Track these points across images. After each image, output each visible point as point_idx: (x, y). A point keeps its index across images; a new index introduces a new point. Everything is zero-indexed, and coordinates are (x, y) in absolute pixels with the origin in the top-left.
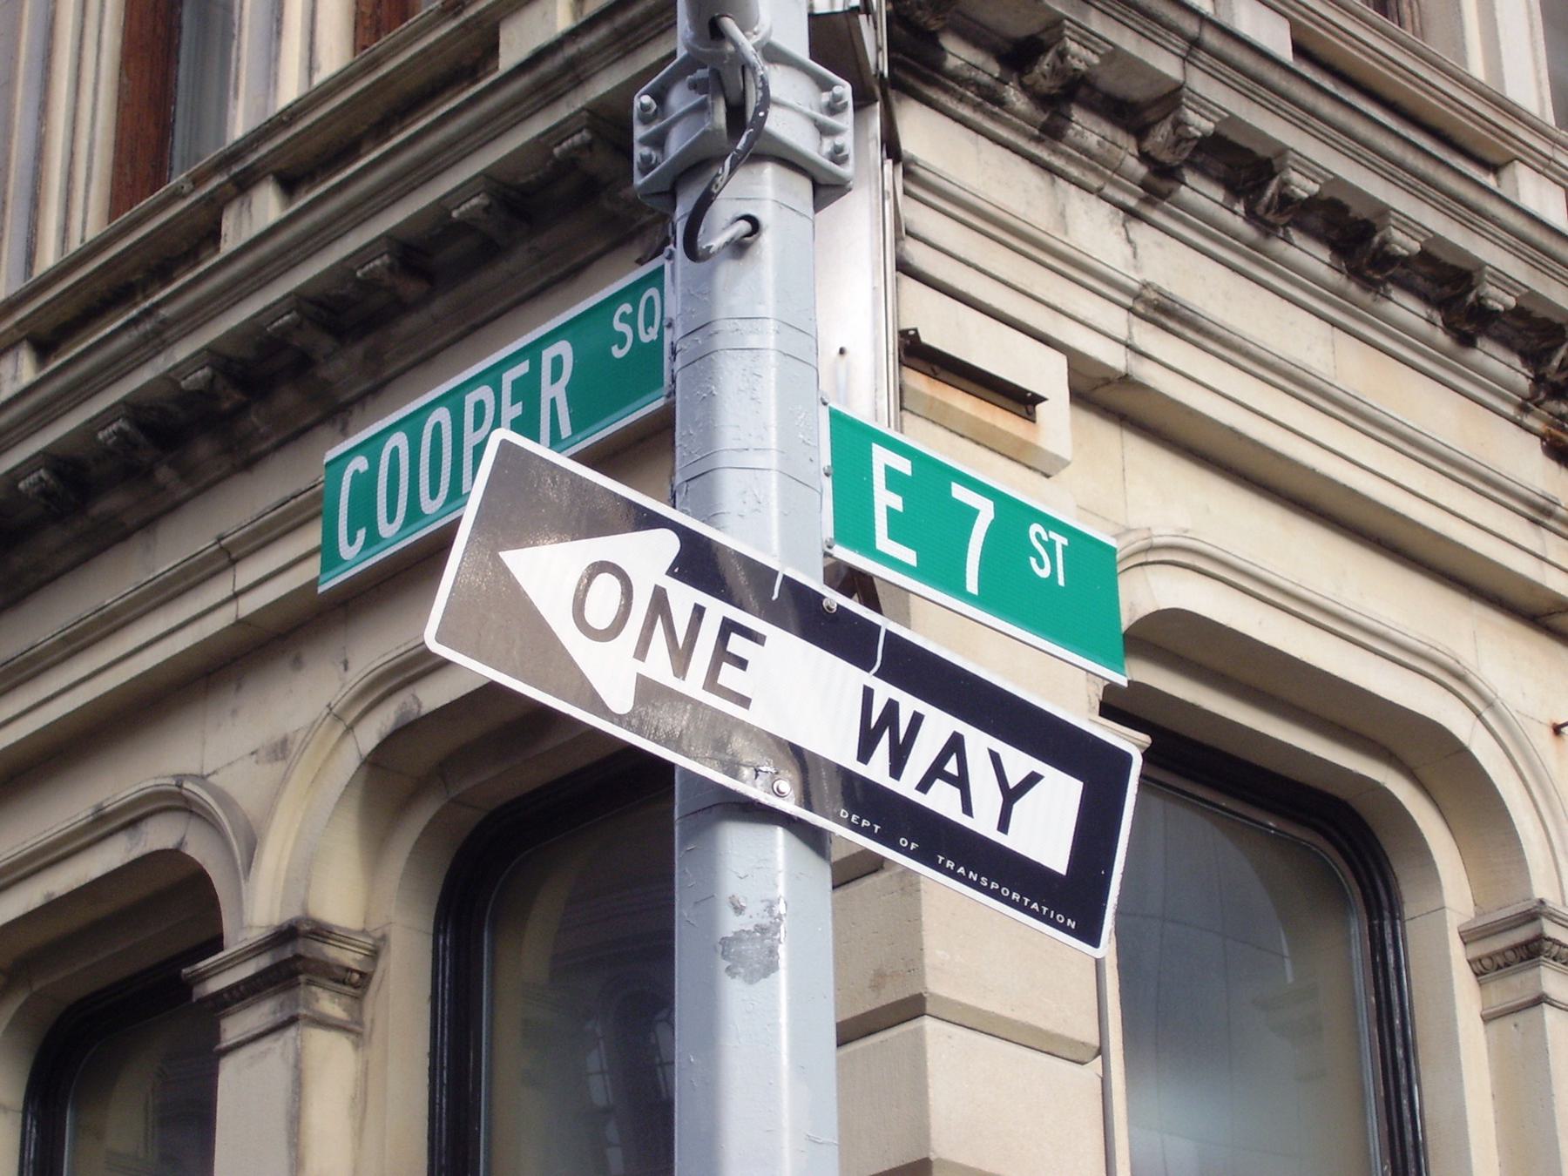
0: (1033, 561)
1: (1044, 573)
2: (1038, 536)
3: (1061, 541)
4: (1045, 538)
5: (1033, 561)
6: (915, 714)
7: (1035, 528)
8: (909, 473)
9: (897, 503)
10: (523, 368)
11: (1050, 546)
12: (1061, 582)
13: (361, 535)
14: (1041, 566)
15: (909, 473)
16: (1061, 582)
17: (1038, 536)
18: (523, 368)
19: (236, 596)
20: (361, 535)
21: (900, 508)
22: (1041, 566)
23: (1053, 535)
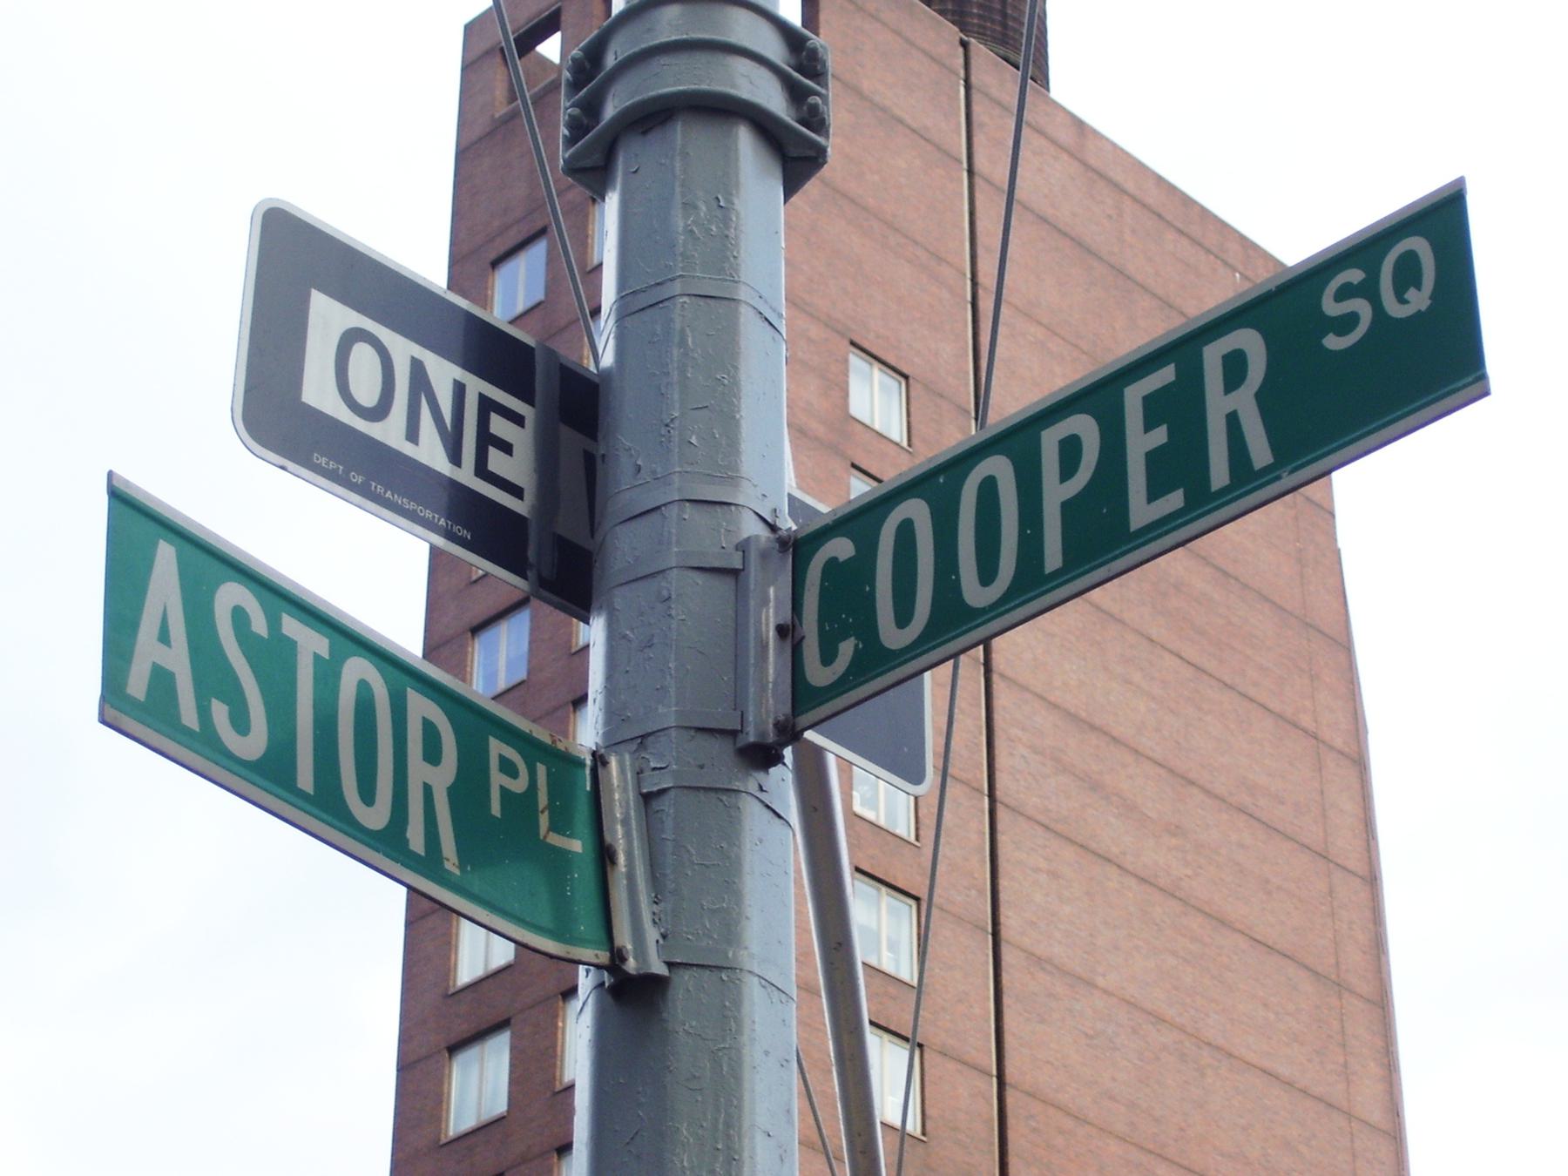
10: (1165, 375)
13: (847, 649)
18: (1165, 375)
20: (847, 649)
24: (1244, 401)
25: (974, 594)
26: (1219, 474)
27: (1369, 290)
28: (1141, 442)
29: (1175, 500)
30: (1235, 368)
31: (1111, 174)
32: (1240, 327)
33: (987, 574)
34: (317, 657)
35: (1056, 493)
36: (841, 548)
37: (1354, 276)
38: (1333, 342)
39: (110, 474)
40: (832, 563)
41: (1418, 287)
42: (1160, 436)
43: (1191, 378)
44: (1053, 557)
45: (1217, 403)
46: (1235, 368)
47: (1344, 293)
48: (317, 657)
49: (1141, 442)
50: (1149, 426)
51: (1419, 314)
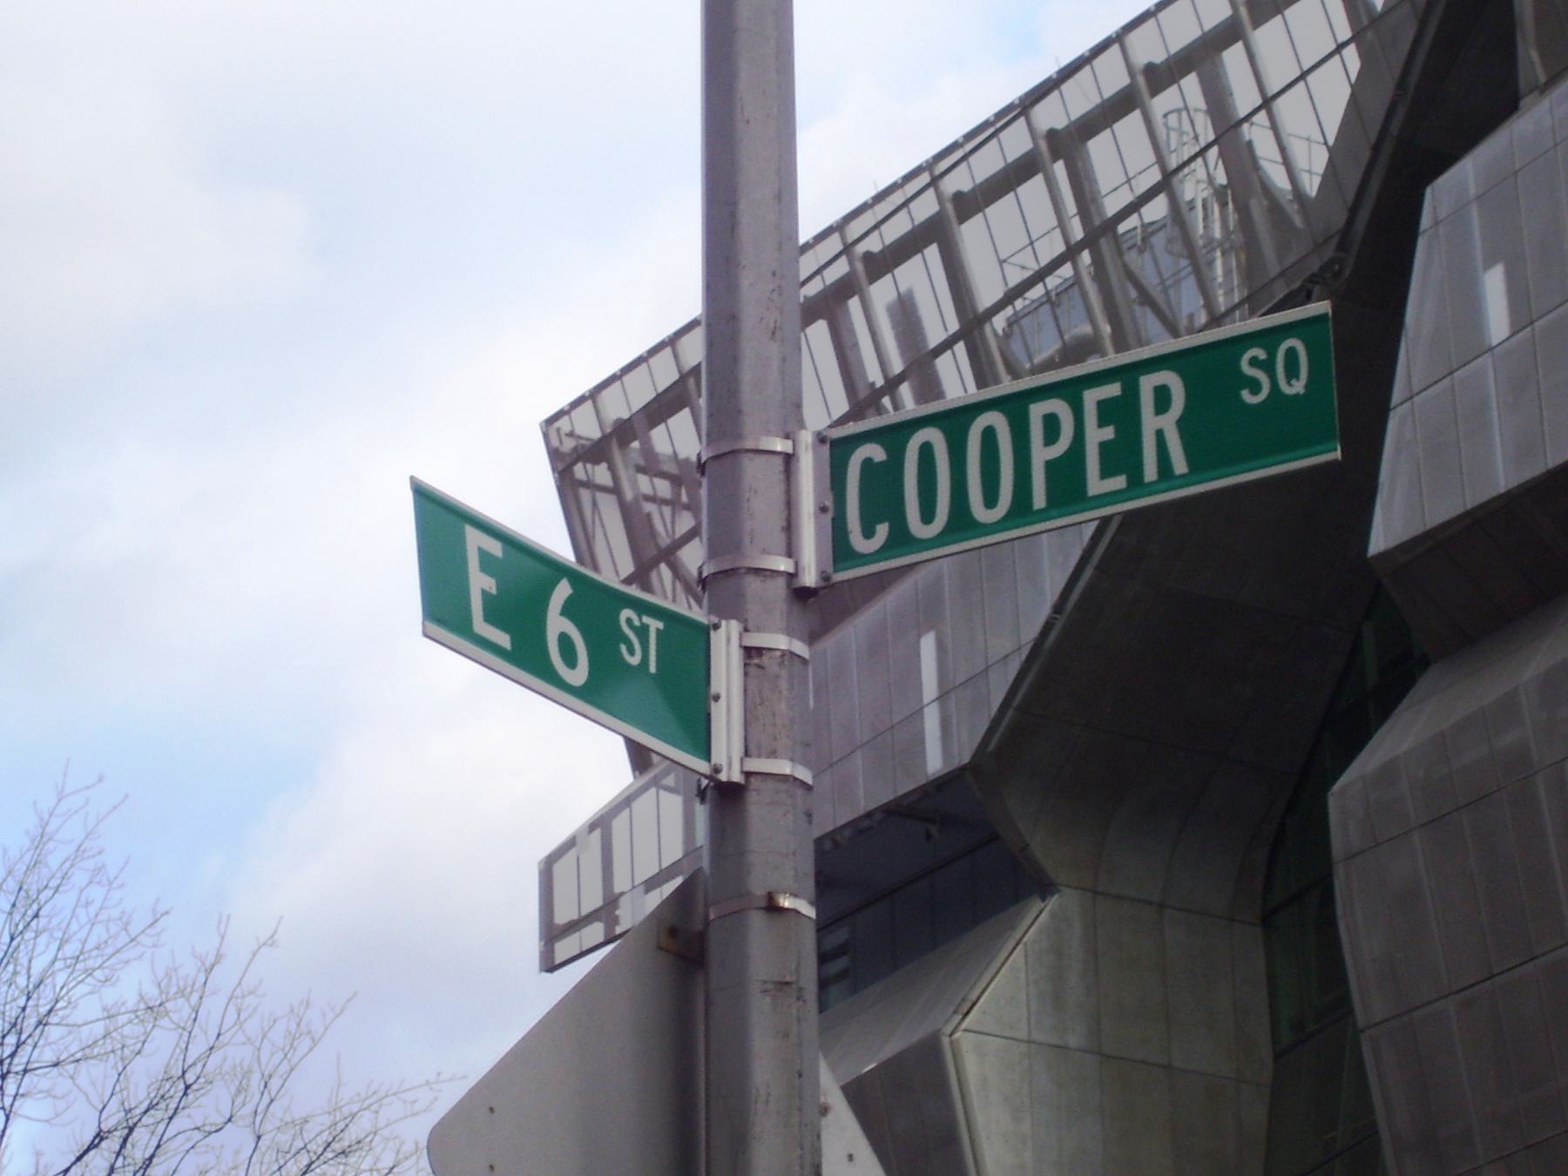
0: (623, 648)
1: (635, 660)
2: (629, 621)
3: (655, 625)
4: (637, 623)
5: (623, 648)
6: (647, 891)
7: (627, 613)
8: (1380, 539)
9: (490, 584)
10: (1113, 390)
11: (642, 632)
12: (653, 669)
13: (882, 530)
14: (632, 652)
15: (1380, 539)
16: (653, 669)
17: (629, 621)
18: (1113, 390)
19: (877, 226)
20: (882, 530)
21: (494, 591)
22: (632, 652)
23: (646, 619)
24: (1169, 422)
25: (980, 513)
26: (1150, 472)
27: (1268, 366)
28: (1096, 435)
29: (1119, 482)
30: (1162, 398)
31: (1406, 53)
32: (1169, 369)
33: (990, 500)
34: (484, 592)
35: (1041, 455)
36: (875, 452)
37: (1261, 354)
38: (1246, 395)
39: (412, 478)
40: (867, 463)
41: (1298, 378)
42: (1108, 433)
43: (1130, 400)
44: (1039, 500)
45: (1150, 422)
46: (1162, 398)
47: (1254, 362)
48: (484, 592)
49: (1096, 435)
50: (1102, 423)
51: (1297, 395)
